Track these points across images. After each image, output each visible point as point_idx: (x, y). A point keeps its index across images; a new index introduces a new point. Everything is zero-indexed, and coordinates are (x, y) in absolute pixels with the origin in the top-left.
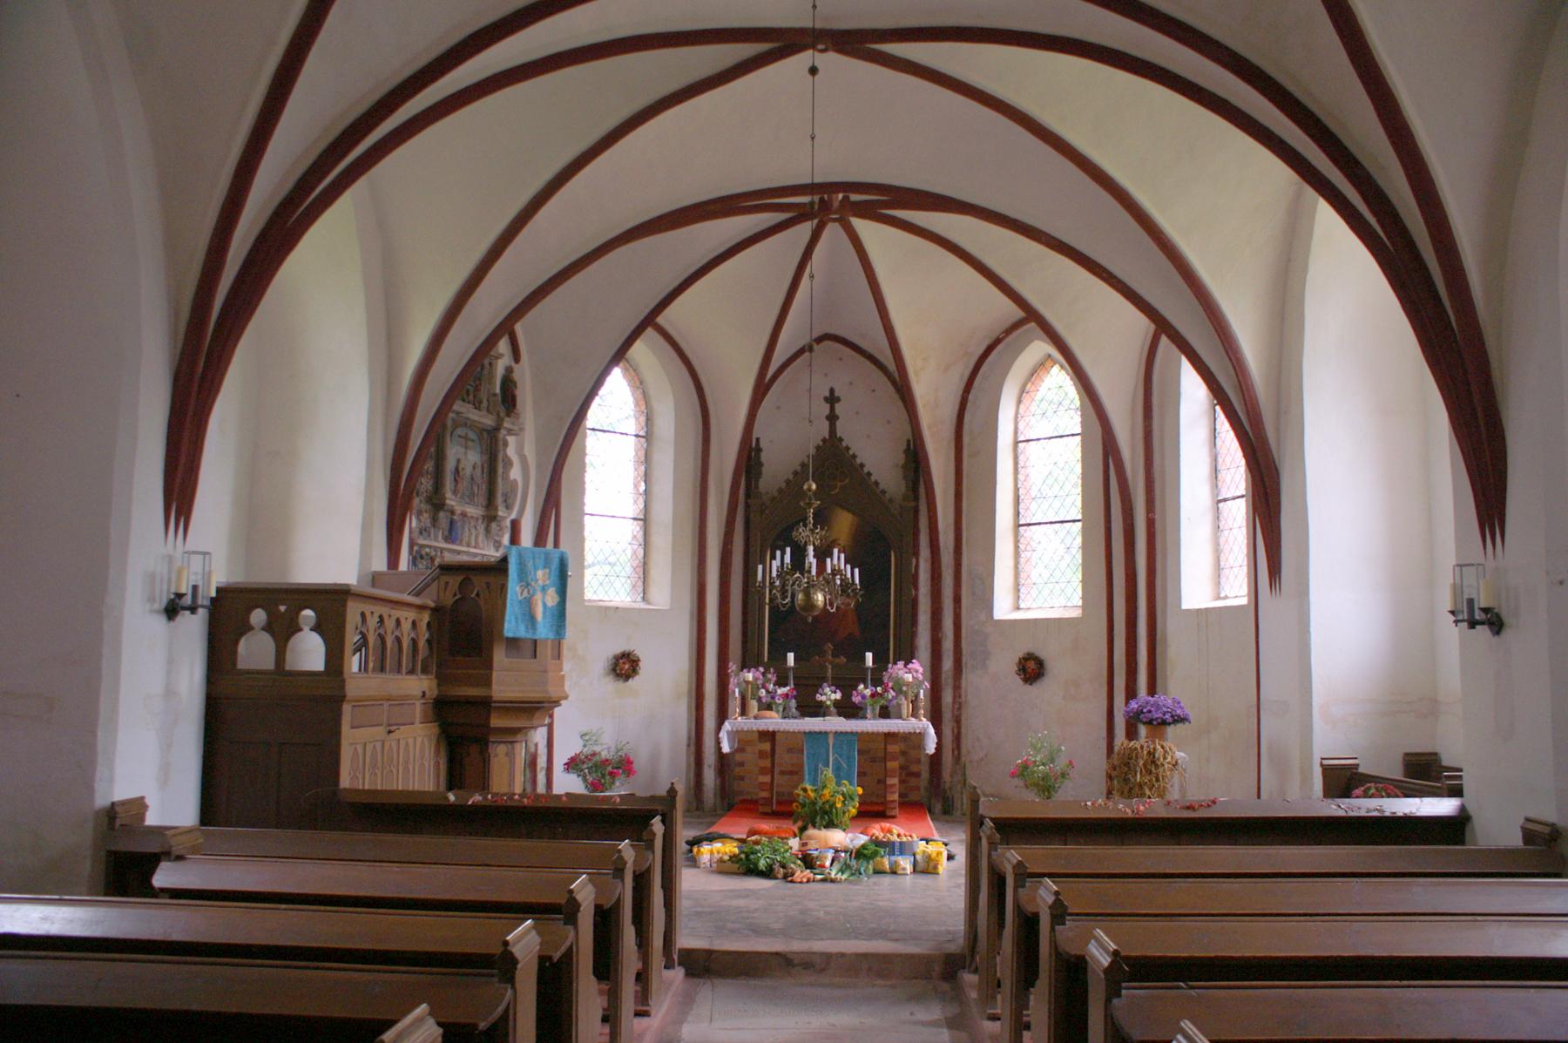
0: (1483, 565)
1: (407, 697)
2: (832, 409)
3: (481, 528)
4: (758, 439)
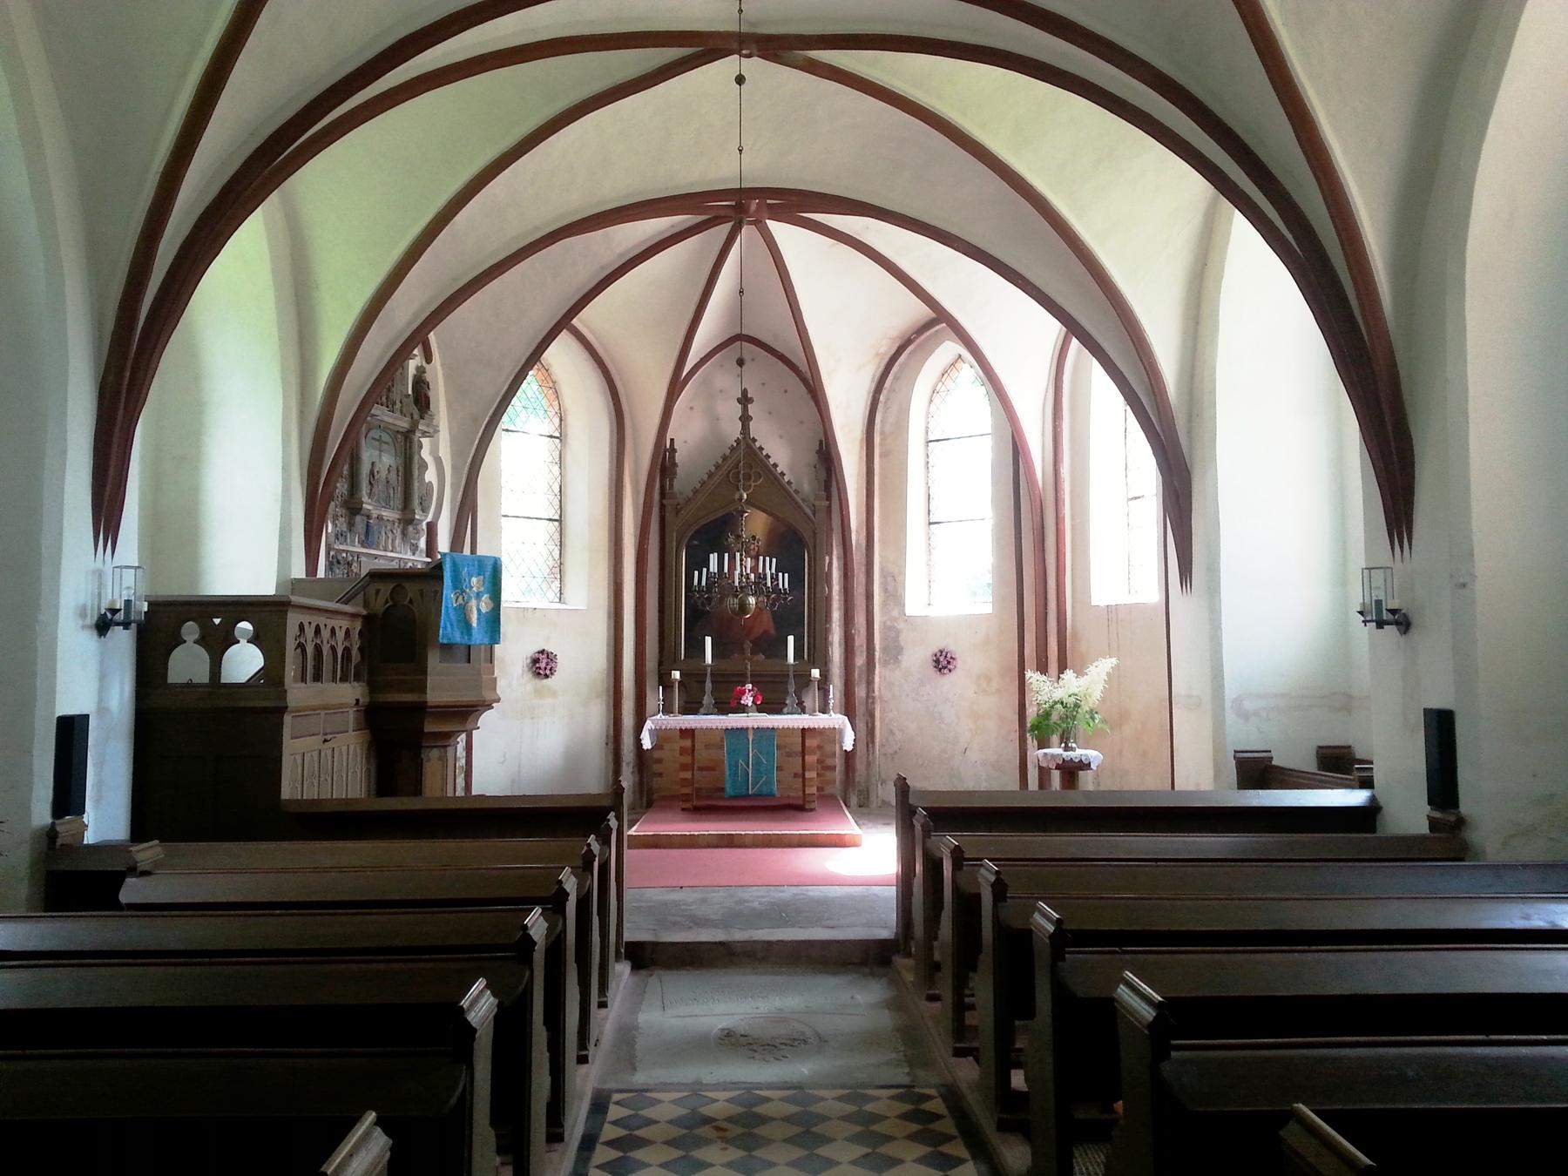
0: (1392, 568)
1: (342, 705)
2: (745, 410)
3: (398, 532)
4: (672, 440)
